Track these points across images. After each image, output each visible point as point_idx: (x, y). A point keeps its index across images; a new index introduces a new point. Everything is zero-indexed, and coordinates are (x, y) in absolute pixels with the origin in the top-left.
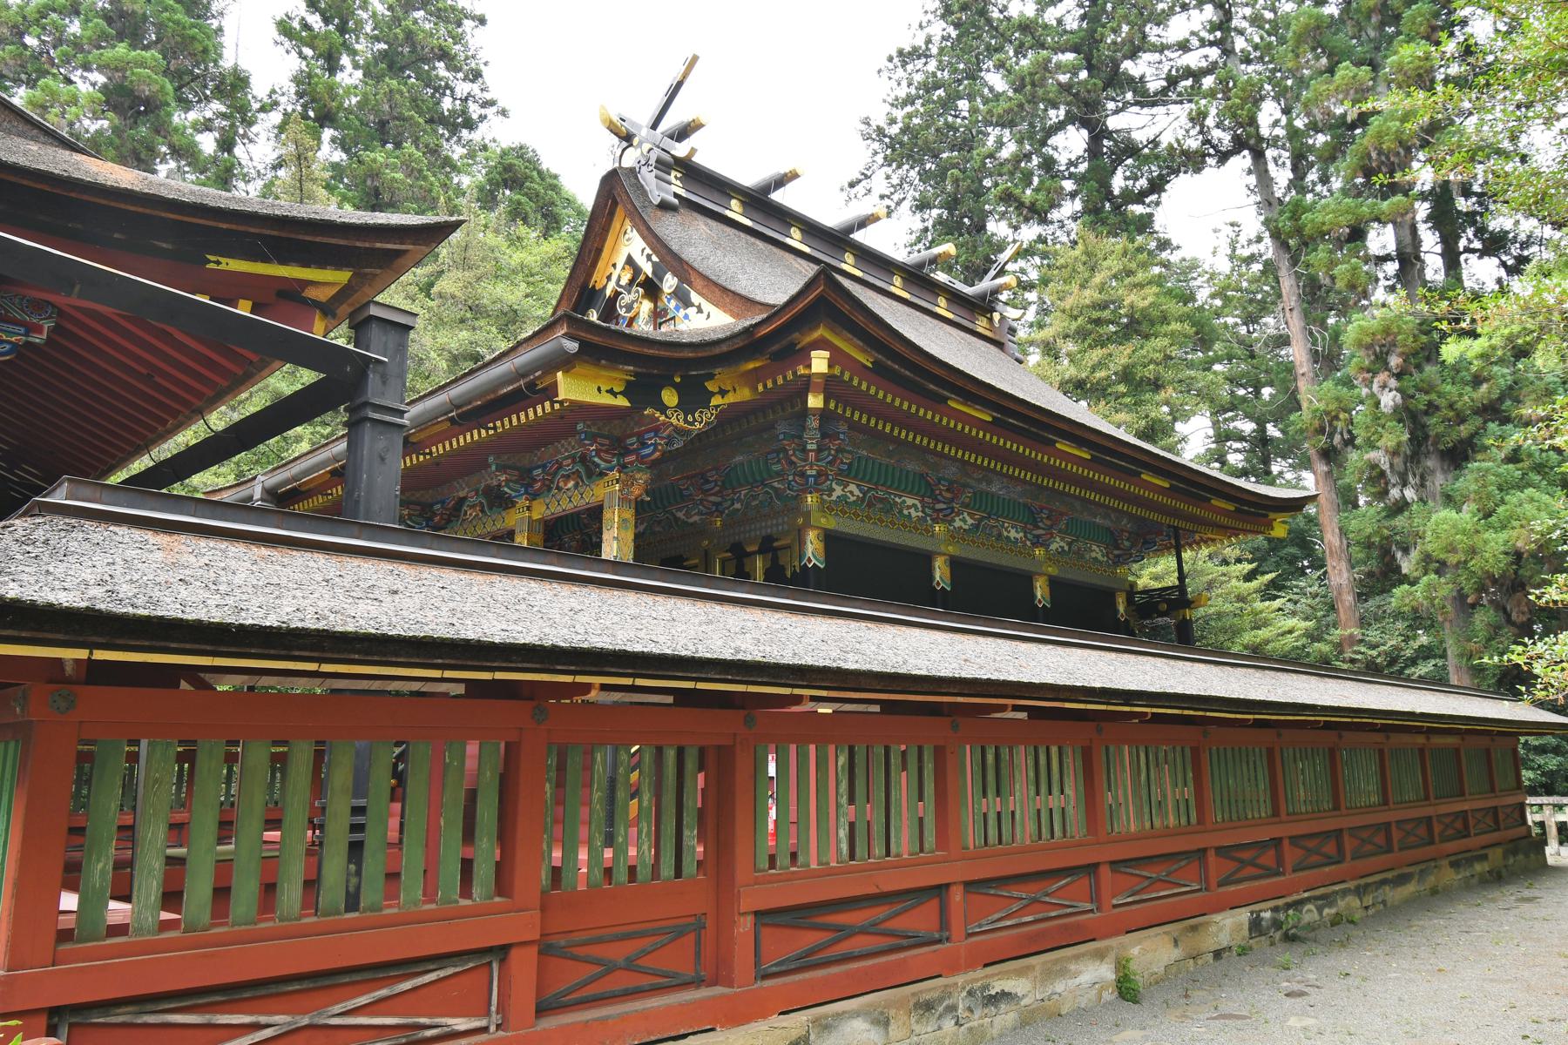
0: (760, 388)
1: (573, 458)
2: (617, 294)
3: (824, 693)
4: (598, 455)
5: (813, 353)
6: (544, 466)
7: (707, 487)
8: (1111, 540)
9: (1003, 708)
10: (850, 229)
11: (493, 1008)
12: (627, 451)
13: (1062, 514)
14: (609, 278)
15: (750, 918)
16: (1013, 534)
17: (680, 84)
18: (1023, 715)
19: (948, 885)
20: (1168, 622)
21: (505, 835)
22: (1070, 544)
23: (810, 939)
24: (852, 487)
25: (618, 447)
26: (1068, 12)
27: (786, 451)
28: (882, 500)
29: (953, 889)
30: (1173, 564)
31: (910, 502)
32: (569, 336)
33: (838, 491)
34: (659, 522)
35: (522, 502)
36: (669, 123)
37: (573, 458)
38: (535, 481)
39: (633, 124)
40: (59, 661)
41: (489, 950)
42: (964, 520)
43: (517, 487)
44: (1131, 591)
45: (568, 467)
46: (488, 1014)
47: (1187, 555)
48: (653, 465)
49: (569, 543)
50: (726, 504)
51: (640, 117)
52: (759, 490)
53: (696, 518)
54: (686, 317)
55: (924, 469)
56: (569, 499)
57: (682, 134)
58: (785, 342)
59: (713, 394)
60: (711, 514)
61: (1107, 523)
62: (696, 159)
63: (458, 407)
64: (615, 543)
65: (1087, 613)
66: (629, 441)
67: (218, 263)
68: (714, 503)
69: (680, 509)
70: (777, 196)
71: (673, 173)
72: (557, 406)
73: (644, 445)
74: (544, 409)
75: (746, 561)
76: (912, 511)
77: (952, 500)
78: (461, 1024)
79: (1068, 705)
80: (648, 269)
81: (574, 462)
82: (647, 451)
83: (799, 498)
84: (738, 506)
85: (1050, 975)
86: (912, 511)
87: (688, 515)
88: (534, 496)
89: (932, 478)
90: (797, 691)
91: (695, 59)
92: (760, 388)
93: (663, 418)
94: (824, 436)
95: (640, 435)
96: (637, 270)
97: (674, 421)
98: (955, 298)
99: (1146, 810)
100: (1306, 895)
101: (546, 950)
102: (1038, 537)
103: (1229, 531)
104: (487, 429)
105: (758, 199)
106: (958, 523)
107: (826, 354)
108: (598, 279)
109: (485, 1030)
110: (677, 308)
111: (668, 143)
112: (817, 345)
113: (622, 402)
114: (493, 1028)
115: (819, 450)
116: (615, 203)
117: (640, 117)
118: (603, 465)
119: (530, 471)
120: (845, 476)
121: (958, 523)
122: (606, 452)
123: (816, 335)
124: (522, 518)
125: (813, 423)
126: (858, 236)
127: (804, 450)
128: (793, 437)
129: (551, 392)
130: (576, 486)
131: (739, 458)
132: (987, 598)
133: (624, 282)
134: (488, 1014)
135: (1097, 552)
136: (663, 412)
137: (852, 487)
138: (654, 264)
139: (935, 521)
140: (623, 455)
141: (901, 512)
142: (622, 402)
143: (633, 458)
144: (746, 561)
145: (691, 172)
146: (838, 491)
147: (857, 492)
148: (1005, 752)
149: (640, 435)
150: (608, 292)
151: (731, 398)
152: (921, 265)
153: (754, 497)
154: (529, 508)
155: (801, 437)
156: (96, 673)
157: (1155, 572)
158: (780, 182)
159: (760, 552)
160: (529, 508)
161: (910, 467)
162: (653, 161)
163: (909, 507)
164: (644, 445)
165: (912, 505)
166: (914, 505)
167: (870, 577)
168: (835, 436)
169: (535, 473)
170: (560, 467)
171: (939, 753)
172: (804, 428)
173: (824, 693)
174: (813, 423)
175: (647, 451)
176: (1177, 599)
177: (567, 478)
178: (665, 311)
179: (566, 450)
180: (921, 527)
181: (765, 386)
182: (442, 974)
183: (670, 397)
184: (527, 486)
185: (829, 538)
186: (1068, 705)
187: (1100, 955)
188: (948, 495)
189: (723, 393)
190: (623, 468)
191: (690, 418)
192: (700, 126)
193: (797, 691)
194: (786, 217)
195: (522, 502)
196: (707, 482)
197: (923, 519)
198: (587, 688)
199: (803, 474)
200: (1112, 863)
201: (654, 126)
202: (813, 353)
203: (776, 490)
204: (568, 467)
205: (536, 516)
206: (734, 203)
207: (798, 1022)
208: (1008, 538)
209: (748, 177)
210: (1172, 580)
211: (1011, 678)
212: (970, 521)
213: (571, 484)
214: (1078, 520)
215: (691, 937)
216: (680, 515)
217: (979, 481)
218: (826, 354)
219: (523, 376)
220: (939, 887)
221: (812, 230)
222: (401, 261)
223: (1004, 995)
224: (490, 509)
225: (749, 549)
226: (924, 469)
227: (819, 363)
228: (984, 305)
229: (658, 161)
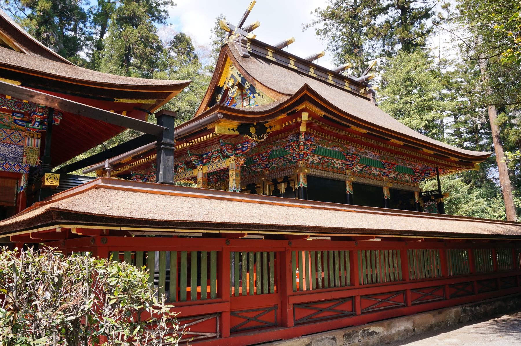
0: (284, 125)
1: (218, 151)
2: (228, 89)
3: (315, 234)
4: (227, 151)
5: (303, 113)
6: (207, 154)
7: (263, 159)
8: (413, 172)
9: (372, 238)
10: (312, 59)
11: (218, 331)
12: (237, 149)
13: (393, 164)
15: (292, 306)
16: (375, 172)
17: (249, 12)
18: (380, 240)
19: (355, 296)
20: (436, 204)
21: (219, 277)
22: (397, 175)
23: (310, 312)
24: (316, 158)
25: (234, 148)
27: (292, 146)
28: (327, 162)
29: (357, 297)
30: (436, 182)
31: (337, 162)
32: (220, 113)
33: (311, 159)
34: (246, 171)
35: (200, 167)
36: (245, 25)
37: (218, 151)
38: (204, 159)
39: (233, 26)
40: (102, 230)
41: (216, 313)
42: (357, 168)
43: (198, 161)
44: (420, 192)
45: (216, 154)
46: (216, 332)
47: (441, 178)
48: (247, 154)
49: (217, 183)
50: (270, 165)
51: (235, 23)
52: (282, 160)
53: (259, 170)
54: (254, 97)
55: (342, 150)
56: (216, 166)
57: (250, 29)
59: (267, 128)
60: (264, 168)
61: (411, 167)
62: (256, 38)
63: (179, 136)
64: (233, 183)
65: (404, 201)
66: (238, 145)
67: (117, 100)
68: (266, 164)
69: (253, 167)
70: (284, 49)
71: (248, 44)
72: (214, 135)
73: (243, 147)
74: (210, 136)
75: (278, 185)
76: (338, 165)
77: (353, 161)
78: (209, 335)
79: (394, 236)
80: (239, 79)
81: (218, 153)
82: (244, 149)
83: (297, 162)
84: (274, 165)
85: (389, 327)
86: (338, 165)
87: (256, 168)
88: (204, 164)
89: (345, 153)
90: (243, 232)
91: (255, 2)
92: (284, 125)
93: (250, 138)
94: (306, 140)
95: (242, 143)
97: (254, 139)
98: (352, 82)
99: (423, 271)
100: (483, 301)
101: (232, 314)
102: (385, 173)
103: (456, 168)
104: (189, 143)
105: (278, 51)
106: (355, 169)
107: (307, 114)
108: (221, 84)
109: (216, 337)
110: (250, 94)
111: (245, 33)
112: (304, 110)
113: (237, 133)
114: (218, 337)
115: (304, 145)
116: (227, 56)
117: (235, 23)
118: (229, 154)
119: (202, 156)
120: (314, 153)
121: (355, 169)
122: (230, 149)
124: (199, 172)
125: (302, 136)
126: (315, 62)
127: (299, 145)
128: (295, 141)
129: (212, 131)
130: (219, 161)
131: (275, 148)
132: (367, 197)
134: (216, 332)
135: (407, 178)
136: (251, 136)
137: (316, 158)
138: (242, 77)
139: (346, 168)
140: (236, 150)
141: (334, 166)
142: (237, 133)
143: (240, 151)
144: (278, 185)
145: (254, 42)
146: (311, 159)
147: (318, 159)
148: (373, 252)
149: (242, 143)
151: (273, 129)
152: (339, 71)
153: (281, 162)
154: (202, 169)
155: (297, 141)
156: (111, 233)
157: (428, 185)
158: (286, 44)
159: (283, 182)
160: (202, 169)
161: (337, 150)
162: (240, 41)
163: (337, 164)
164: (243, 147)
165: (338, 163)
166: (339, 163)
167: (323, 191)
168: (310, 140)
169: (204, 156)
170: (213, 154)
171: (351, 253)
172: (298, 138)
173: (315, 234)
174: (302, 136)
175: (244, 149)
176: (437, 195)
177: (216, 158)
178: (246, 94)
179: (215, 148)
180: (341, 171)
181: (285, 124)
182: (204, 320)
183: (252, 130)
184: (201, 161)
185: (309, 178)
186: (394, 236)
187: (408, 320)
188: (351, 159)
189: (271, 128)
190: (236, 155)
191: (260, 137)
192: (257, 27)
193: (243, 232)
194: (287, 56)
195: (200, 167)
196: (263, 157)
197: (342, 168)
198: (244, 234)
199: (298, 154)
200: (411, 290)
201: (240, 27)
202: (303, 113)
203: (288, 159)
204: (216, 154)
205: (205, 171)
207: (306, 340)
208: (373, 174)
209: (273, 43)
210: (437, 187)
212: (359, 168)
213: (217, 160)
214: (398, 169)
215: (273, 312)
216: (253, 168)
217: (363, 154)
218: (307, 114)
219: (204, 126)
220: (352, 297)
221: (298, 60)
222: (171, 95)
223: (374, 332)
224: (188, 169)
225: (279, 181)
226: (342, 150)
227: (305, 116)
228: (364, 84)
229: (242, 40)
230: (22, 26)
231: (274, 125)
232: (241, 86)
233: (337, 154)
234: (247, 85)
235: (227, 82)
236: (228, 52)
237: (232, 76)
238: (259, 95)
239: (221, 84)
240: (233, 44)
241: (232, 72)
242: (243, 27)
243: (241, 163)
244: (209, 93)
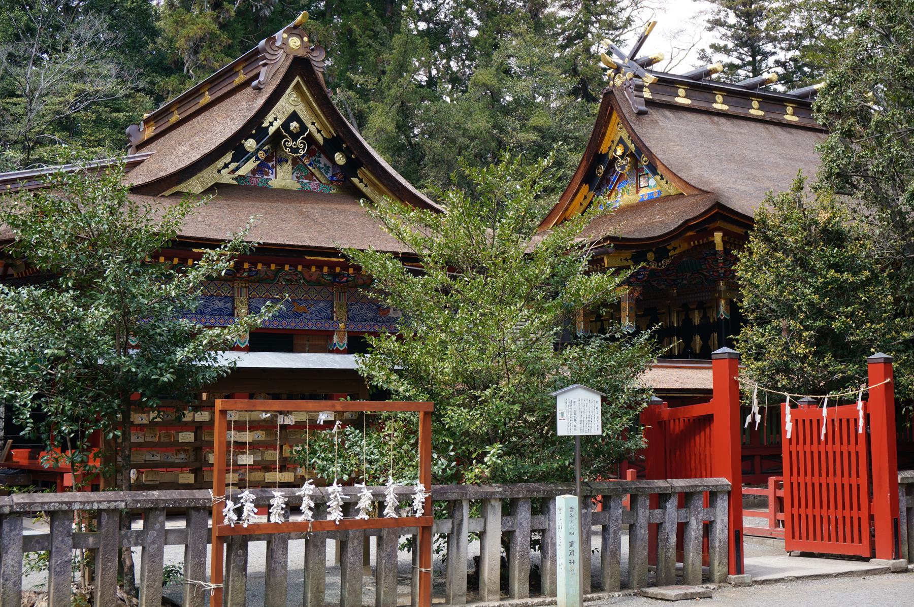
17: (646, 37)
50: (679, 281)
53: (663, 286)
84: (685, 282)
96: (626, 148)
108: (604, 149)
116: (612, 109)
151: (678, 251)
201: (632, 59)
216: (654, 283)
225: (691, 307)
230: (490, 565)
231: (679, 248)
232: (635, 158)
233: (708, 472)
234: (644, 161)
235: (613, 148)
236: (613, 103)
237: (621, 141)
238: (662, 178)
239: (604, 149)
240: (621, 89)
241: (620, 134)
242: (637, 57)
243: (636, 294)
244: (584, 163)
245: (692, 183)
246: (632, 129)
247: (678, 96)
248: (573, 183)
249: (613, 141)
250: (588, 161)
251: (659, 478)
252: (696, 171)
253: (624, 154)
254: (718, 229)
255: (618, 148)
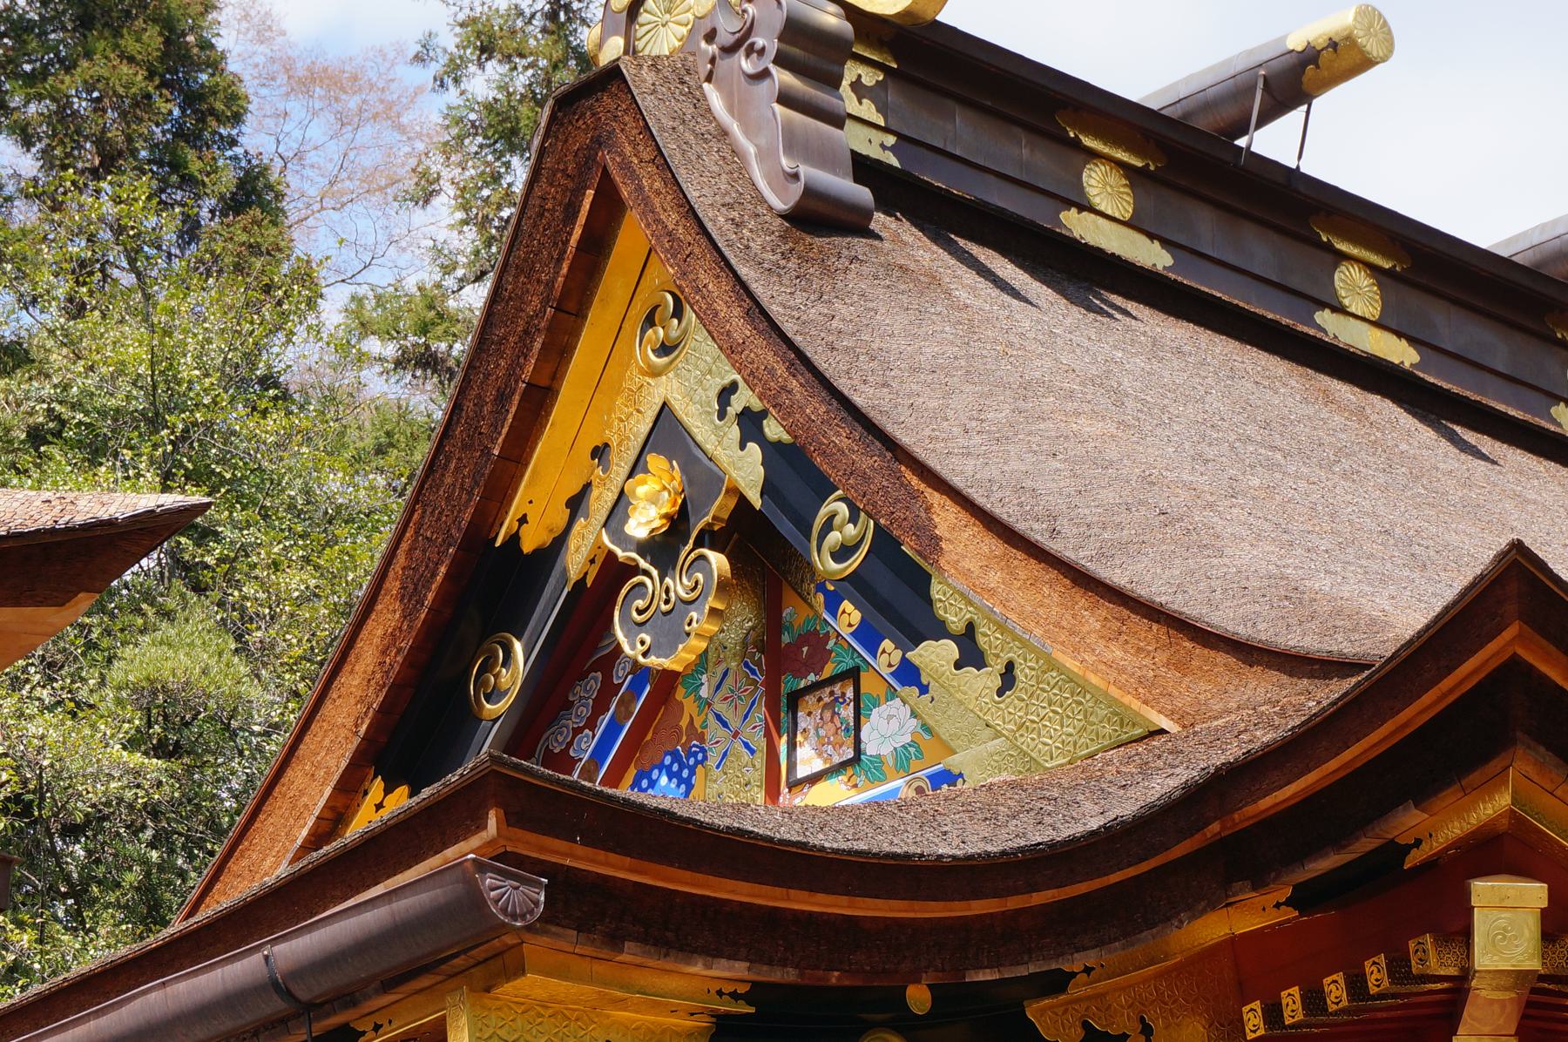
5: (1483, 890)
14: (576, 504)
26: (542, 3)
58: (1366, 844)
71: (852, 71)
80: (746, 470)
96: (700, 474)
105: (1199, 158)
107: (1535, 893)
108: (532, 512)
110: (868, 636)
116: (610, 208)
123: (1494, 806)
133: (643, 522)
138: (773, 451)
150: (576, 561)
158: (1293, 82)
178: (817, 642)
194: (1313, 214)
202: (1483, 890)
206: (1100, 184)
211: (1450, 595)
218: (1535, 893)
232: (761, 548)
234: (837, 536)
235: (602, 499)
237: (667, 432)
238: (971, 655)
239: (532, 512)
240: (681, 74)
241: (666, 389)
244: (387, 616)
245: (1225, 618)
246: (758, 313)
247: (1085, 207)
248: (296, 776)
249: (600, 453)
250: (410, 596)
251: (1119, 294)
252: (1250, 557)
253: (678, 523)
254: (1499, 851)
255: (643, 488)
